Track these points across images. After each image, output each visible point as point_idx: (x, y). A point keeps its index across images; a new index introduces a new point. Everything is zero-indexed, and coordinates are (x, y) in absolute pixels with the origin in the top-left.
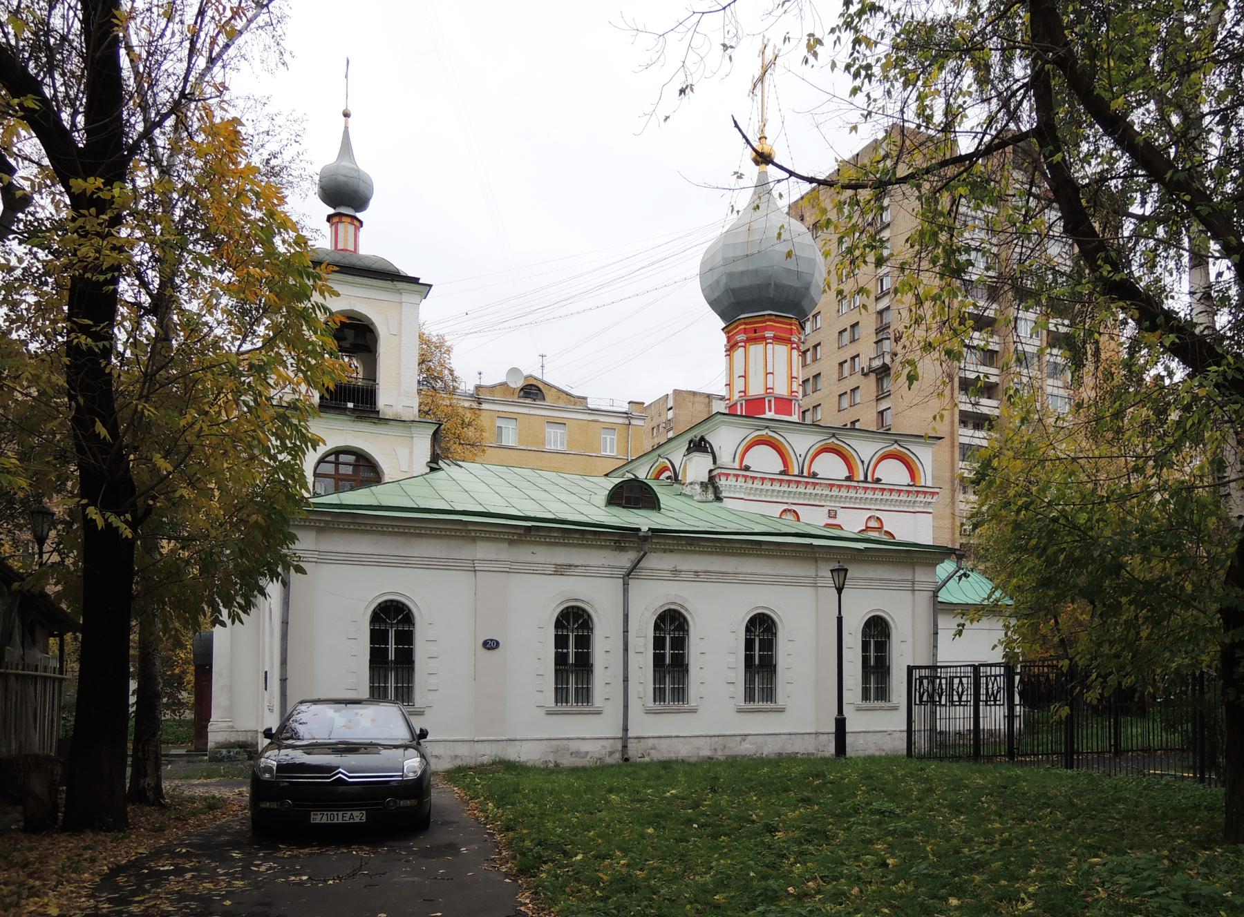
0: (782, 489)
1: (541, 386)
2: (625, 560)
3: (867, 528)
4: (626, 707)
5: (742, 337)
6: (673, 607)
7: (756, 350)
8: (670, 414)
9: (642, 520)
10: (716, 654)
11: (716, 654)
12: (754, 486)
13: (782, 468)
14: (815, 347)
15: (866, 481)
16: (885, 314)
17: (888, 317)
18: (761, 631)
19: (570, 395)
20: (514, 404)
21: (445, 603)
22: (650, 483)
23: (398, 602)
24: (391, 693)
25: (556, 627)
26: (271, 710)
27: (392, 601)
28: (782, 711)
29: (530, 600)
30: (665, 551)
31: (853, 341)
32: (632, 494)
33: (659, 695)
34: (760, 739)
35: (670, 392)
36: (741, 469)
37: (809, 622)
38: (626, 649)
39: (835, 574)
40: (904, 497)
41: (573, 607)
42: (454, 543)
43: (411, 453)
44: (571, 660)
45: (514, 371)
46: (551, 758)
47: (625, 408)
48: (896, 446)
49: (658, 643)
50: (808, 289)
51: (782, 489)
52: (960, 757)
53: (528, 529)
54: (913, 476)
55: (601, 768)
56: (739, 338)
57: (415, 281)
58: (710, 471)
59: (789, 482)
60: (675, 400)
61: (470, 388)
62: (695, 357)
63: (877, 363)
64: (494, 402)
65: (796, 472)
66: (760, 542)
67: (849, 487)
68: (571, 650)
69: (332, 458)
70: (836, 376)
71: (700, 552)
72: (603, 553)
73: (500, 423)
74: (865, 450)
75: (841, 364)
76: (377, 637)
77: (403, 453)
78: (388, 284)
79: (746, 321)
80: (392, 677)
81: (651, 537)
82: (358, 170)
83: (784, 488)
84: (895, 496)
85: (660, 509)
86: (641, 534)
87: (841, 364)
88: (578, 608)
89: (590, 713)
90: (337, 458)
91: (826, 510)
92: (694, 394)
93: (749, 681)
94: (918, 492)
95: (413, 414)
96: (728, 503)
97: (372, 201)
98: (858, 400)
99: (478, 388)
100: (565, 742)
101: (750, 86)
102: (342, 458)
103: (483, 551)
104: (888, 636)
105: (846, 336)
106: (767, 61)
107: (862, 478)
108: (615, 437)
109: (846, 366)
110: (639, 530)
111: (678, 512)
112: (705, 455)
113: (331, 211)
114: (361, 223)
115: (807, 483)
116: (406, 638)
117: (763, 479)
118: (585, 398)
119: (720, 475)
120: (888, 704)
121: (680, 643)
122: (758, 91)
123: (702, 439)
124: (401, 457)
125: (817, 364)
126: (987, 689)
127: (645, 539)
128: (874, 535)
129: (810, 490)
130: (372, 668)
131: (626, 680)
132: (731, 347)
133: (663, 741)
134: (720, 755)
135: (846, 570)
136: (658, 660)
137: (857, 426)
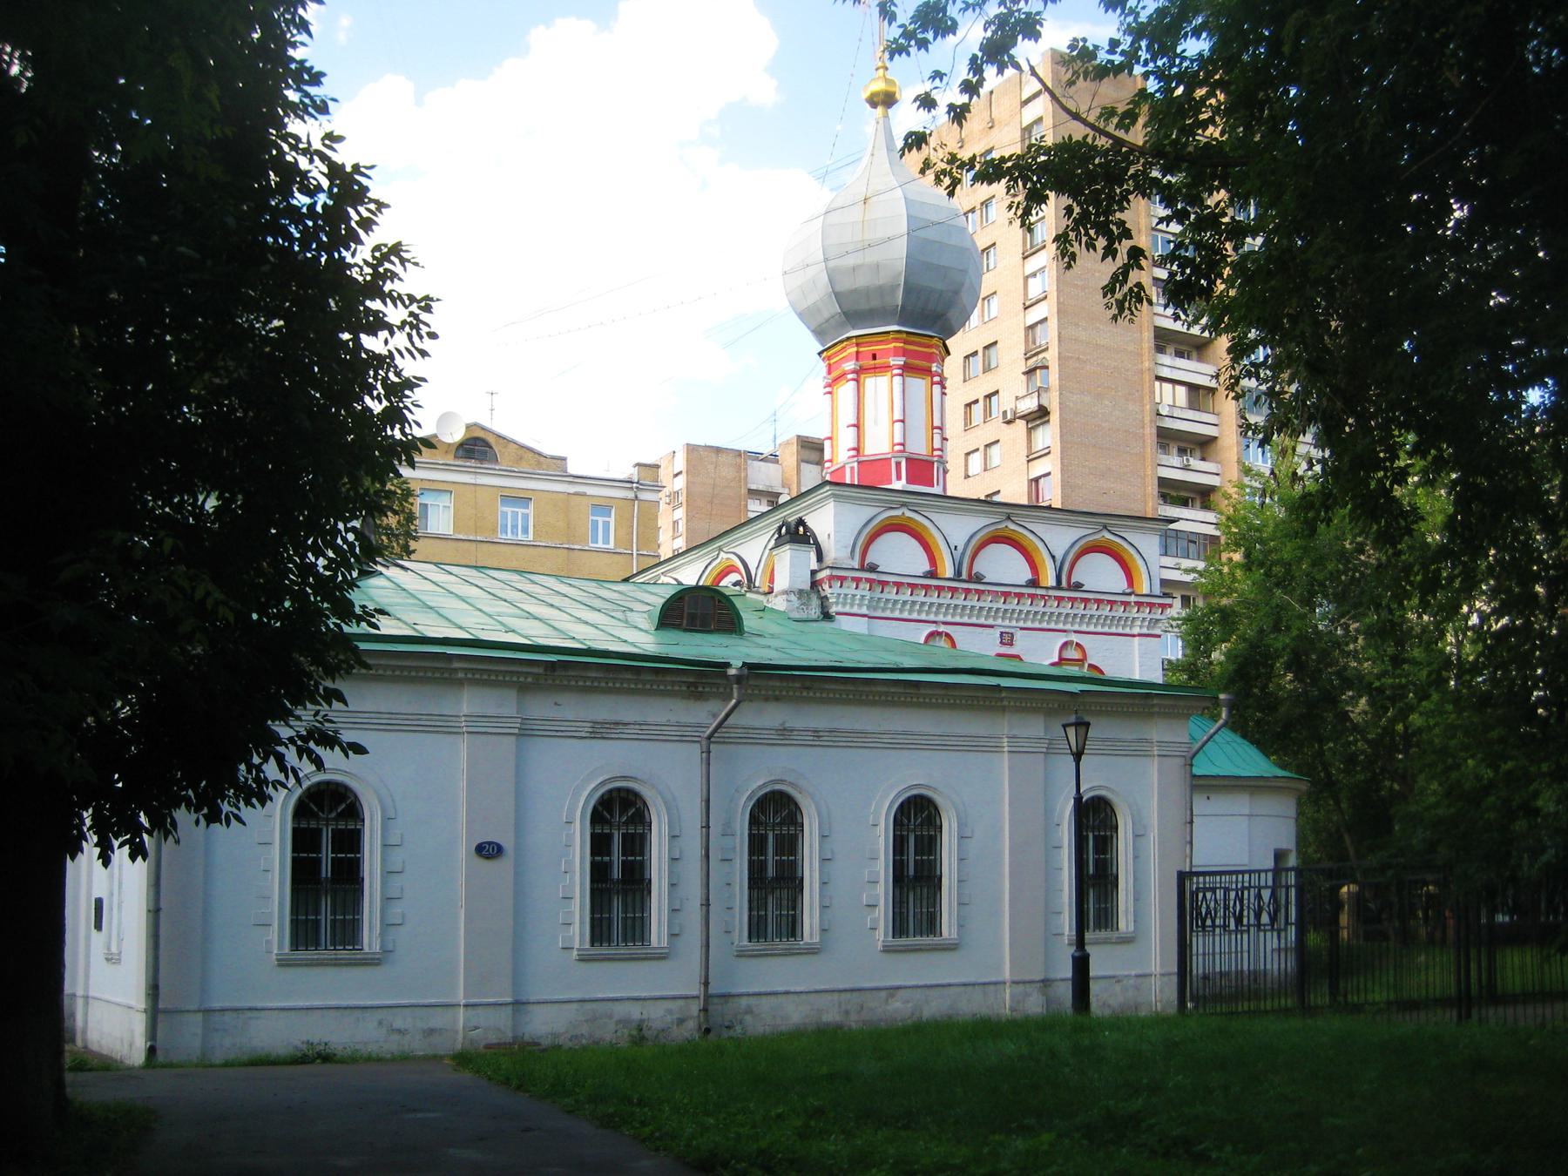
1: (491, 440)
2: (704, 714)
3: (1062, 661)
6: (778, 787)
7: (881, 388)
10: (847, 862)
12: (885, 596)
13: (927, 567)
15: (1058, 586)
18: (917, 820)
19: (540, 454)
20: (447, 467)
30: (766, 699)
31: (987, 369)
32: (699, 609)
33: (757, 929)
36: (862, 568)
37: (1002, 807)
41: (619, 790)
44: (616, 873)
46: (584, 1030)
50: (956, 293)
51: (928, 600)
52: (1266, 1012)
55: (686, 1050)
59: (940, 589)
63: (1030, 404)
65: (949, 573)
66: (917, 684)
67: (1032, 596)
68: (617, 857)
71: (822, 701)
72: (671, 703)
75: (969, 405)
80: (326, 904)
81: (748, 677)
84: (1106, 611)
86: (732, 672)
88: (628, 791)
92: (718, 450)
94: (1139, 604)
96: (845, 623)
100: (610, 1004)
108: (612, 520)
109: (978, 410)
110: (727, 665)
111: (772, 635)
112: (803, 547)
115: (968, 591)
116: (350, 841)
117: (898, 585)
118: (564, 459)
120: (1115, 934)
121: (790, 845)
123: (801, 522)
129: (973, 601)
132: (833, 382)
133: (764, 1000)
134: (853, 1022)
135: (1087, 725)
137: (996, 499)
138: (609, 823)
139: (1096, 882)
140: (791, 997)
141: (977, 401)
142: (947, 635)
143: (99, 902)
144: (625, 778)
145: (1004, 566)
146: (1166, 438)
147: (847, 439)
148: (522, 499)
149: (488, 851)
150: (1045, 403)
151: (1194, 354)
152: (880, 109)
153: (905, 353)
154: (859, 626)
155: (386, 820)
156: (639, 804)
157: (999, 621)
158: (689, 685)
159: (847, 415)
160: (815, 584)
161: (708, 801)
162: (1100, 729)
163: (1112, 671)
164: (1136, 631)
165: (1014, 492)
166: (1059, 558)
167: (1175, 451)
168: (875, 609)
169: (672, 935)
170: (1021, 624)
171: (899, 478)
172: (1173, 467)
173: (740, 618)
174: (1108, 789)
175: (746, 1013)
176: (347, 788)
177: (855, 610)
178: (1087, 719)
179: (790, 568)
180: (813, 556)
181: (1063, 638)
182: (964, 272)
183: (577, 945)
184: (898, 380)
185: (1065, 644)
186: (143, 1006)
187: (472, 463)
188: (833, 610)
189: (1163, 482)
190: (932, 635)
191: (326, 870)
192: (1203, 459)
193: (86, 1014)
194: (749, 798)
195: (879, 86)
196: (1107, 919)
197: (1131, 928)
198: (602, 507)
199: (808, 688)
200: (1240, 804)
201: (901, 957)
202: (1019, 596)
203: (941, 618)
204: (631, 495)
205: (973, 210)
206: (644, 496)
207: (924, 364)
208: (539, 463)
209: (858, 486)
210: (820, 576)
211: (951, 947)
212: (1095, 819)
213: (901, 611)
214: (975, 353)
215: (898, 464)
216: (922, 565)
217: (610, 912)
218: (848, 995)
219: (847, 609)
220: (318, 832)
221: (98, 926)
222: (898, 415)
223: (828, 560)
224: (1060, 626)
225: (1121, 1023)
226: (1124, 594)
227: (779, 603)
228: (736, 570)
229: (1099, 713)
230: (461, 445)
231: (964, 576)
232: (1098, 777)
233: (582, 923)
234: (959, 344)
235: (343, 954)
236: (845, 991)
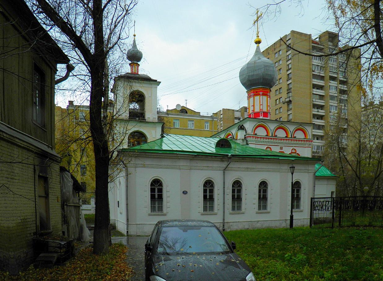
0: (266, 141)
2: (224, 165)
3: (292, 152)
4: (224, 212)
5: (252, 94)
7: (257, 98)
8: (222, 116)
10: (250, 194)
11: (250, 194)
14: (280, 98)
16: (290, 85)
17: (291, 86)
18: (263, 185)
19: (195, 112)
20: (178, 115)
21: (172, 179)
23: (158, 179)
24: (157, 208)
25: (204, 187)
26: (121, 213)
27: (156, 179)
28: (269, 213)
29: (198, 177)
31: (280, 93)
33: (233, 209)
34: (262, 222)
35: (222, 109)
37: (279, 182)
38: (224, 193)
40: (303, 142)
45: (178, 105)
48: (301, 126)
49: (233, 191)
51: (266, 141)
54: (305, 136)
57: (156, 81)
59: (269, 138)
60: (223, 112)
61: (165, 110)
63: (287, 100)
64: (172, 114)
65: (271, 135)
66: (263, 158)
74: (291, 128)
75: (276, 100)
76: (152, 190)
77: (153, 132)
78: (148, 82)
79: (254, 89)
80: (157, 203)
82: (138, 50)
83: (267, 140)
84: (300, 142)
85: (231, 148)
86: (229, 156)
87: (276, 100)
88: (210, 180)
89: (162, 215)
91: (280, 147)
92: (229, 110)
93: (259, 203)
94: (307, 141)
95: (156, 120)
96: (250, 146)
98: (281, 111)
99: (167, 110)
101: (253, 22)
103: (182, 163)
104: (300, 188)
105: (278, 92)
106: (258, 16)
107: (290, 137)
111: (236, 149)
112: (243, 130)
113: (130, 62)
114: (139, 65)
115: (274, 139)
116: (160, 191)
117: (261, 138)
119: (248, 136)
121: (239, 191)
122: (256, 24)
123: (242, 125)
124: (152, 134)
127: (230, 158)
128: (294, 154)
129: (275, 141)
130: (151, 201)
131: (224, 203)
132: (249, 97)
135: (294, 167)
136: (233, 196)
139: (296, 198)
140: (240, 223)
141: (278, 99)
142: (270, 148)
143: (118, 201)
146: (315, 106)
147: (252, 108)
149: (185, 193)
151: (320, 89)
156: (212, 183)
159: (252, 104)
160: (245, 138)
162: (297, 167)
163: (302, 155)
165: (284, 119)
167: (316, 108)
168: (256, 142)
172: (315, 111)
173: (231, 145)
174: (299, 180)
175: (231, 226)
179: (241, 135)
180: (245, 132)
182: (274, 75)
186: (126, 223)
189: (314, 115)
190: (267, 148)
191: (156, 197)
192: (322, 110)
193: (117, 224)
195: (257, 40)
196: (298, 207)
198: (207, 122)
200: (325, 182)
201: (260, 214)
202: (284, 139)
203: (269, 144)
204: (212, 119)
205: (277, 62)
207: (266, 93)
208: (195, 114)
211: (269, 213)
212: (296, 186)
215: (261, 113)
216: (265, 134)
217: (207, 205)
218: (250, 222)
221: (118, 207)
223: (247, 133)
225: (301, 228)
226: (304, 139)
228: (231, 135)
230: (181, 110)
231: (273, 136)
232: (297, 177)
234: (273, 89)
235: (160, 213)
236: (249, 221)
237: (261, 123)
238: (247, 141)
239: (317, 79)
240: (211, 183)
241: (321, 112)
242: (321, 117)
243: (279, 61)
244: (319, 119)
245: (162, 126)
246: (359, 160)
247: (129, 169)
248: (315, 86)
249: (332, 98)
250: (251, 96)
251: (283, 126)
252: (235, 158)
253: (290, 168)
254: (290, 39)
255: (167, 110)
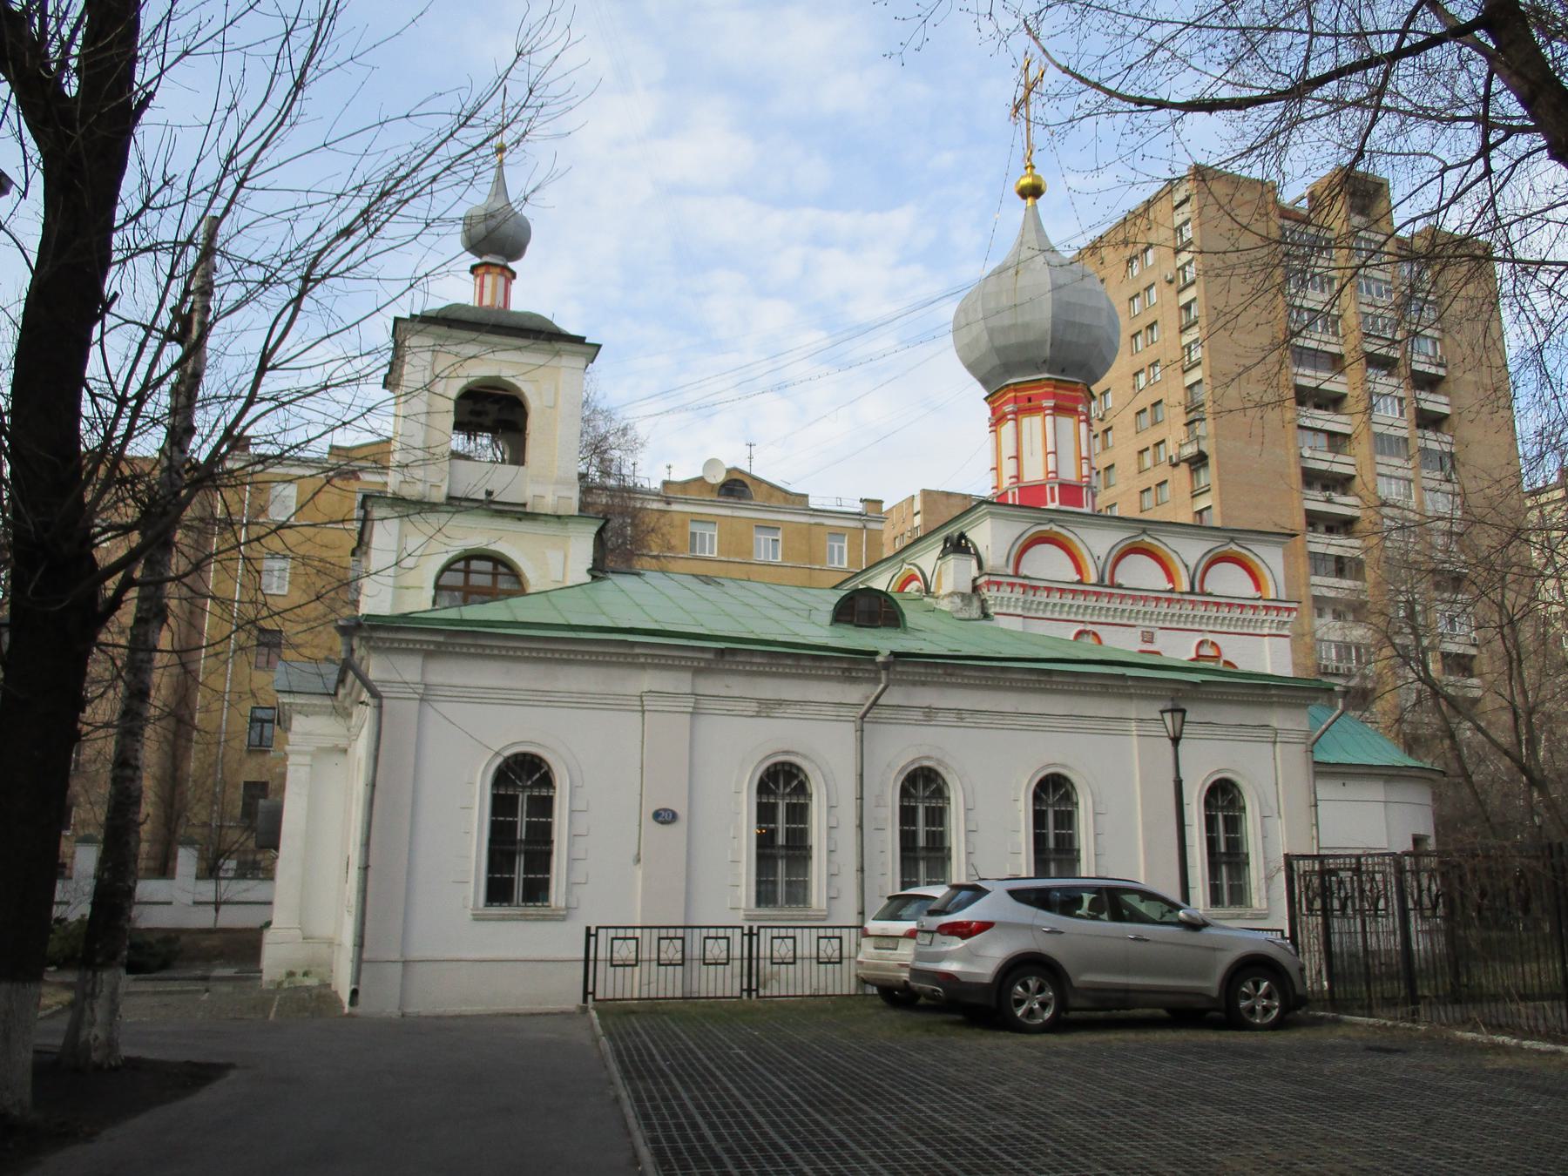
1: (747, 481)
2: (857, 694)
3: (1199, 657)
7: (1033, 425)
9: (882, 642)
15: (1192, 592)
19: (786, 492)
20: (712, 503)
22: (895, 596)
30: (914, 684)
31: (1155, 423)
35: (917, 492)
39: (1168, 717)
41: (783, 764)
42: (616, 673)
43: (566, 557)
47: (859, 508)
53: (721, 652)
56: (1009, 408)
57: (580, 340)
58: (975, 580)
62: (953, 442)
63: (1189, 451)
64: (686, 502)
69: (461, 565)
70: (1134, 468)
73: (697, 528)
75: (1141, 452)
76: (502, 805)
77: (554, 558)
83: (1080, 601)
84: (1236, 613)
86: (879, 659)
88: (791, 765)
89: (545, 918)
90: (467, 565)
91: (1139, 631)
92: (948, 495)
94: (1267, 608)
95: (574, 508)
97: (529, 248)
102: (475, 565)
105: (1146, 419)
108: (845, 545)
110: (876, 653)
111: (928, 632)
113: (477, 261)
114: (514, 275)
117: (1049, 589)
118: (806, 496)
120: (1249, 911)
121: (1066, 819)
123: (962, 536)
125: (1108, 453)
126: (125, 764)
129: (1115, 603)
132: (997, 420)
135: (1183, 711)
138: (916, 798)
142: (1095, 634)
144: (787, 752)
145: (1141, 574)
146: (1311, 478)
148: (772, 528)
149: (664, 817)
150: (1204, 448)
152: (1030, 200)
153: (1054, 396)
154: (1015, 625)
155: (573, 788)
156: (802, 777)
157: (1140, 622)
158: (844, 670)
159: (1008, 449)
161: (862, 775)
163: (1243, 666)
164: (1266, 631)
166: (1192, 565)
169: (831, 899)
170: (1160, 624)
171: (1053, 500)
172: (1316, 501)
176: (541, 760)
177: (1011, 611)
178: (1183, 706)
179: (953, 575)
180: (974, 563)
181: (1198, 638)
183: (743, 905)
184: (1049, 419)
185: (1201, 643)
187: (731, 500)
188: (992, 611)
190: (1080, 634)
194: (900, 772)
195: (1027, 181)
197: (1265, 906)
198: (837, 534)
199: (951, 675)
200: (1375, 791)
203: (1087, 618)
204: (860, 525)
205: (1137, 295)
206: (872, 526)
209: (1020, 506)
210: (980, 581)
213: (1053, 612)
214: (1144, 410)
215: (1052, 489)
219: (1004, 610)
220: (775, 806)
222: (1050, 448)
224: (1196, 627)
227: (945, 605)
228: (916, 579)
229: (1194, 700)
231: (1107, 582)
233: (748, 885)
237: (1046, 527)
238: (983, 602)
239: (1315, 367)
240: (796, 776)
241: (1343, 505)
242: (1344, 525)
243: (1148, 289)
244: (1338, 533)
245: (595, 529)
246: (1519, 700)
247: (385, 702)
248: (1305, 396)
249: (1385, 444)
250: (1005, 415)
251: (1148, 539)
252: (910, 669)
253: (1162, 712)
254: (1187, 200)
255: (666, 484)
